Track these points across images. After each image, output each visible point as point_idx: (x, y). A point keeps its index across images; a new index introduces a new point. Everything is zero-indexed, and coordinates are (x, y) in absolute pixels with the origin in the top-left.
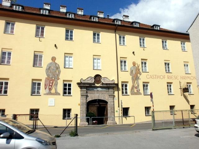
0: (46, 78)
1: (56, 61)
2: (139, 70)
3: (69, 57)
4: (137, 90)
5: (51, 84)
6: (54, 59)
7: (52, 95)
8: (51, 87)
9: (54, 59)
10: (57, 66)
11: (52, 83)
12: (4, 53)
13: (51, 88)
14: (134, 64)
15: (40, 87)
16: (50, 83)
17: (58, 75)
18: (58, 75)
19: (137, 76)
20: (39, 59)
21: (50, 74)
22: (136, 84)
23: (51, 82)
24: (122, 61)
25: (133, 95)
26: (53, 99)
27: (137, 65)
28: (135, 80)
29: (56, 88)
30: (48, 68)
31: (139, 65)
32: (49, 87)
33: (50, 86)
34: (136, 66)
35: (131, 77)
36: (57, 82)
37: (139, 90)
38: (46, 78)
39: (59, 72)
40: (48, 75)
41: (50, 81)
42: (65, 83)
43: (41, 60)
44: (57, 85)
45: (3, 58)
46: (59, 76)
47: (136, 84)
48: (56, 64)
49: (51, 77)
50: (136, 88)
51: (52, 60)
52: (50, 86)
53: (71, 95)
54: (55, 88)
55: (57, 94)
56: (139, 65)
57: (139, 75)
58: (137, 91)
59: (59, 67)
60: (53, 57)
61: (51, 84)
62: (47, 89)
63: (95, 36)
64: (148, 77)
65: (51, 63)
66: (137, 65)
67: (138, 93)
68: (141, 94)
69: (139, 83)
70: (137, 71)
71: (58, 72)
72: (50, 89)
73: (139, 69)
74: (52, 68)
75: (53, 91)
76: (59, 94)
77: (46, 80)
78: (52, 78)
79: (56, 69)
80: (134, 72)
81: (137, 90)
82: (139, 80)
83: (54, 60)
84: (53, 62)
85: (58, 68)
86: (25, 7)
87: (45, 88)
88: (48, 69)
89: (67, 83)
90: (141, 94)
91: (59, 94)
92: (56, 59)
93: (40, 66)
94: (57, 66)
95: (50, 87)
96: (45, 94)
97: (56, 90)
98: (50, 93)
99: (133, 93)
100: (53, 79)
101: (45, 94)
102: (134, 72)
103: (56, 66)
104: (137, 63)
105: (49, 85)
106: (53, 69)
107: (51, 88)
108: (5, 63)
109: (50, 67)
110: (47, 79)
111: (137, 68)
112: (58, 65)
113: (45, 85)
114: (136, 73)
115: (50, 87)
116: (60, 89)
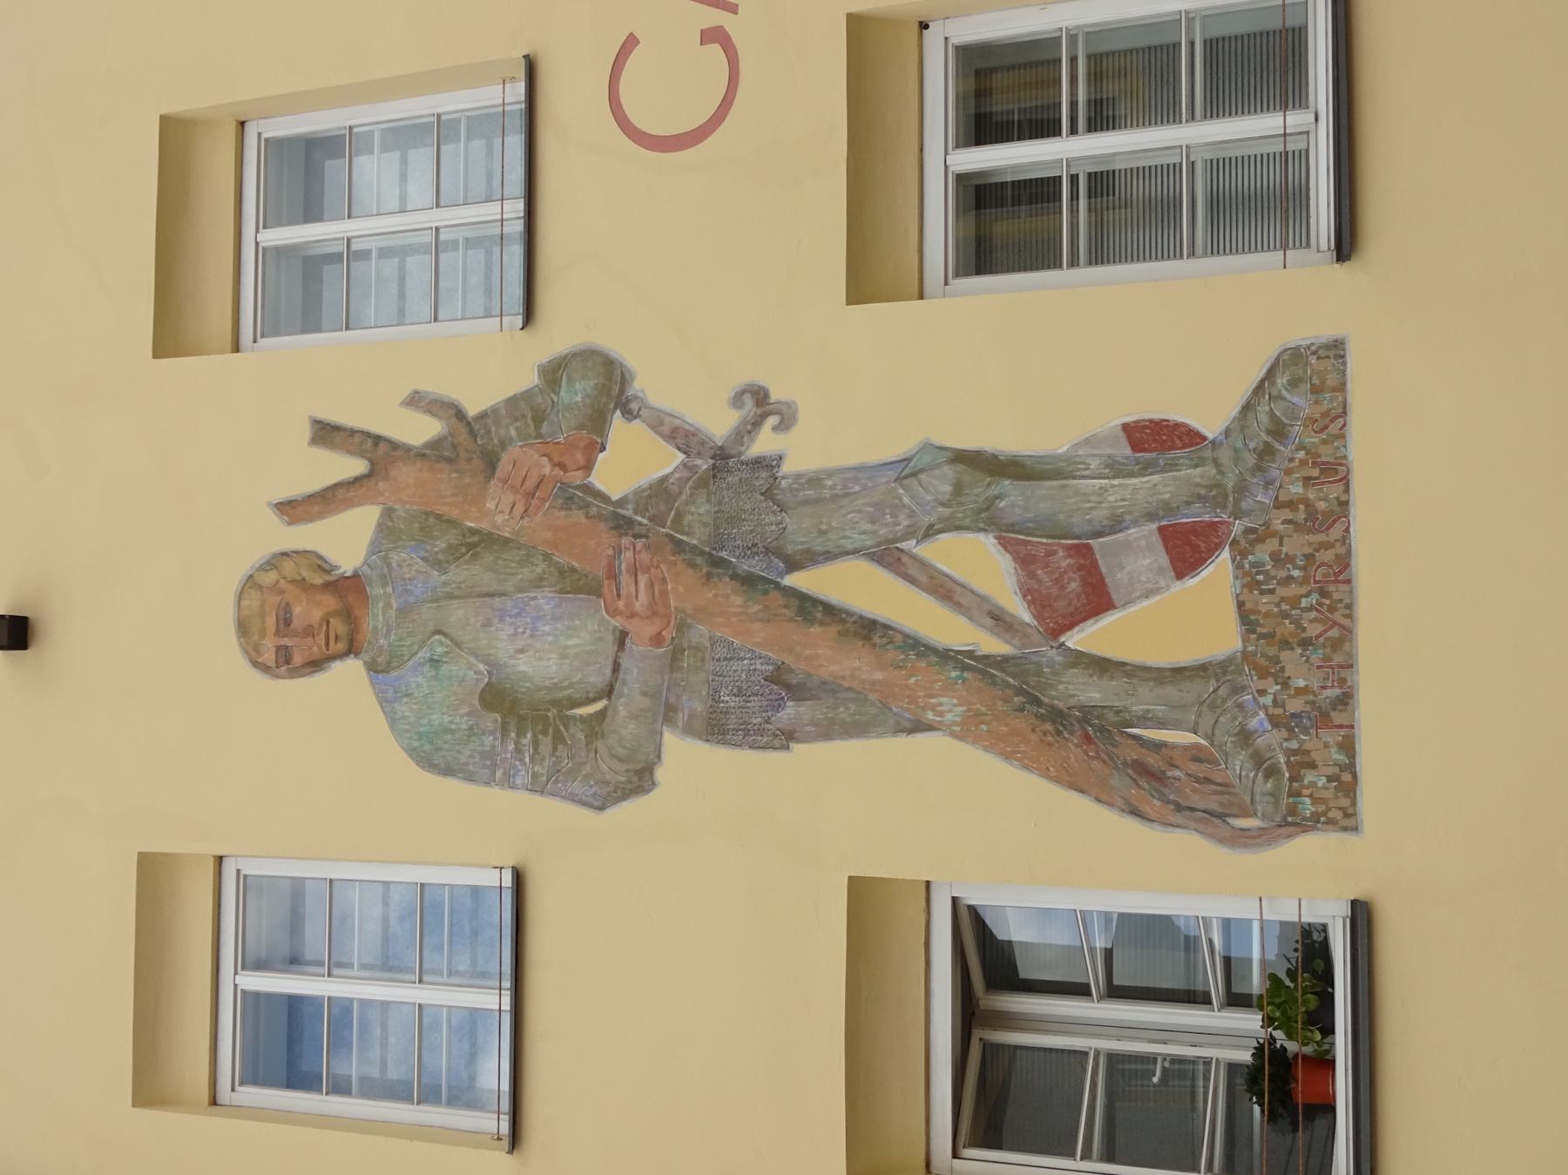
2: (470, 444)
4: (1136, 557)
14: (304, 622)
19: (641, 519)
22: (944, 589)
24: (979, 196)
25: (1333, 710)
27: (326, 500)
28: (809, 608)
31: (326, 433)
34: (345, 541)
35: (685, 759)
37: (1155, 439)
47: (944, 589)
50: (1098, 600)
56: (326, 433)
57: (629, 463)
58: (1187, 550)
63: (1038, 191)
64: (671, 89)
66: (326, 500)
67: (1268, 492)
68: (1309, 381)
69: (905, 470)
70: (497, 510)
73: (436, 453)
80: (550, 647)
81: (1136, 557)
82: (801, 451)
86: (1021, 943)
90: (1309, 381)
99: (1278, 742)
102: (550, 647)
104: (293, 510)
111: (431, 521)
114: (576, 584)
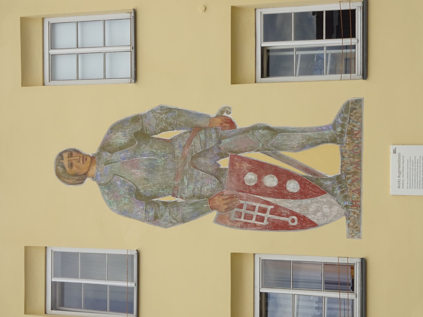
0: (219, 220)
1: (90, 148)
3: (52, 47)
5: (271, 181)
6: (72, 167)
7: (359, 165)
8: (290, 176)
9: (72, 167)
10: (120, 138)
11: (261, 168)
12: (61, 297)
13: (301, 180)
15: (296, 14)
16: (259, 189)
17: (193, 124)
18: (196, 130)
20: (83, 277)
21: (188, 192)
23: (251, 178)
26: (393, 159)
29: (298, 139)
30: (139, 208)
32: (293, 196)
33: (282, 185)
36: (254, 128)
38: (219, 220)
39: (171, 116)
40: (200, 205)
41: (247, 189)
42: (252, 63)
43: (89, 263)
44: (274, 131)
45: (96, 300)
46: (201, 123)
48: (106, 147)
49: (209, 186)
51: (79, 179)
52: (282, 185)
53: (356, 5)
54: (303, 147)
55: (347, 128)
59: (136, 119)
60: (59, 175)
61: (271, 181)
62: (310, 207)
65: (107, 187)
71: (173, 127)
72: (312, 186)
74: (138, 174)
75: (326, 161)
76: (353, 110)
77: (234, 224)
78: (218, 173)
79: (146, 149)
83: (80, 167)
84: (93, 171)
85: (138, 131)
87: (305, 223)
88: (148, 204)
89: (254, 41)
91: (353, 110)
92: (72, 152)
93: (134, 263)
94: (120, 138)
95: (293, 186)
96: (355, 229)
97: (313, 139)
98: (347, 188)
100: (224, 163)
101: (355, 229)
103: (121, 148)
105: (280, 192)
106: (152, 168)
107: (301, 180)
108: (129, 290)
109: (138, 195)
110: (231, 214)
112: (113, 129)
113: (276, 226)
115: (293, 186)
116: (300, 102)
